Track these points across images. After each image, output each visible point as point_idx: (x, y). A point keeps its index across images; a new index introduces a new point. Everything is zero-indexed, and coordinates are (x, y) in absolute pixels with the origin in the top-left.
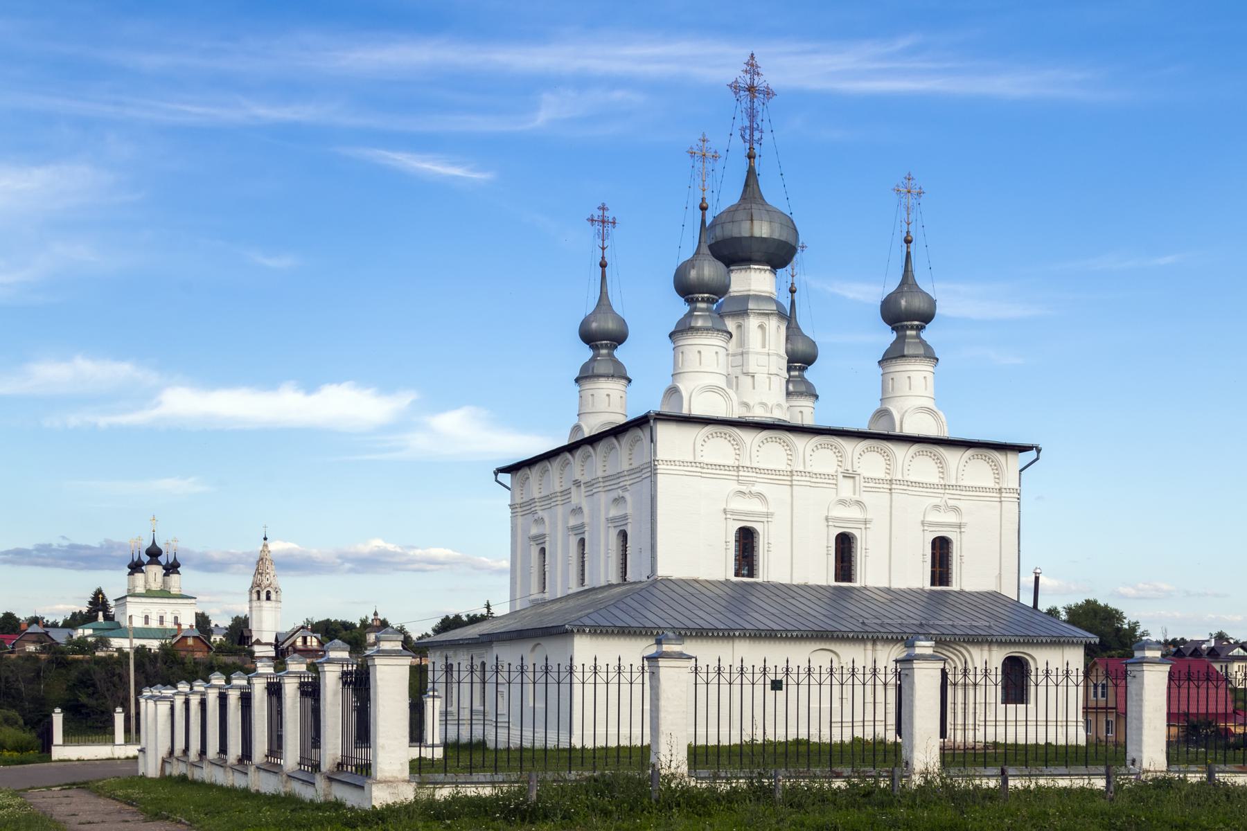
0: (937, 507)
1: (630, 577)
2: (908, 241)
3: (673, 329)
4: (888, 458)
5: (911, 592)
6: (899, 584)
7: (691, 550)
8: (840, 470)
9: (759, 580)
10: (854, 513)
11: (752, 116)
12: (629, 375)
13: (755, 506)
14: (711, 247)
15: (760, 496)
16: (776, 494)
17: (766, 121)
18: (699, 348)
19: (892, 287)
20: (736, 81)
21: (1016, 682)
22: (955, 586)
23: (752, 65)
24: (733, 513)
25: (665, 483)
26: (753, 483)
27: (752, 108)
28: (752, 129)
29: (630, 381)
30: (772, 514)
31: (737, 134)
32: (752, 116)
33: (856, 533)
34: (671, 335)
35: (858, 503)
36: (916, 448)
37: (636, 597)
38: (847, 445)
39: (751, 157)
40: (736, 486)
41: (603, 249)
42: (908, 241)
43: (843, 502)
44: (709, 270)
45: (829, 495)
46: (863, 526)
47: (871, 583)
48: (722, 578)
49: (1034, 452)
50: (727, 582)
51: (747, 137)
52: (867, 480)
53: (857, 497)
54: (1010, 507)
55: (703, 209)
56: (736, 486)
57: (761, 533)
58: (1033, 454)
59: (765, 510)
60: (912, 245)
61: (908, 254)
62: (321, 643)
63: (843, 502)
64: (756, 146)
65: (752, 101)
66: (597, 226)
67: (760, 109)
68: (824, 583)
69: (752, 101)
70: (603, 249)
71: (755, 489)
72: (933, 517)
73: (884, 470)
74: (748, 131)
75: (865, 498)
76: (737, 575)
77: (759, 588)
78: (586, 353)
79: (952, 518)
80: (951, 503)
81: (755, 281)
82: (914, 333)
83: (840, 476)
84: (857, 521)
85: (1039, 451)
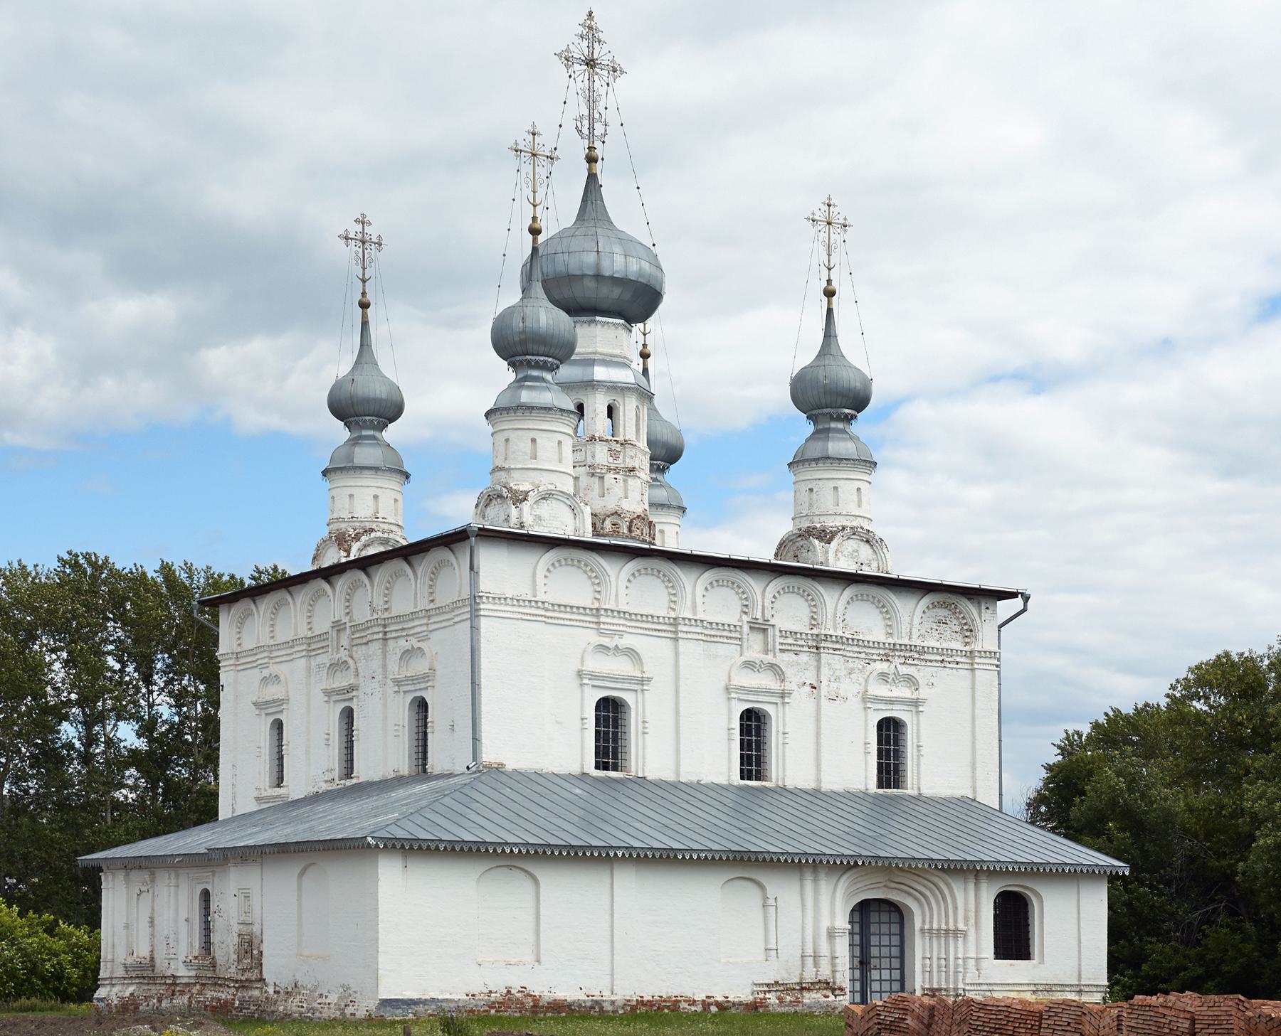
0: (883, 676)
1: (436, 762)
2: (829, 293)
3: (490, 406)
4: (597, 580)
5: (849, 796)
7: (530, 725)
9: (909, 792)
11: (592, 101)
12: (407, 468)
13: (620, 666)
14: (546, 284)
15: (631, 653)
16: (654, 650)
17: (612, 108)
18: (533, 434)
19: (344, 367)
20: (568, 50)
21: (1013, 936)
22: (910, 790)
23: (590, 28)
24: (593, 676)
25: (496, 632)
26: (621, 634)
27: (591, 89)
28: (591, 119)
29: (407, 476)
30: (649, 679)
31: (570, 126)
32: (592, 101)
33: (628, 698)
35: (772, 666)
36: (710, 575)
37: (457, 795)
38: (754, 584)
39: (591, 160)
40: (593, 638)
41: (364, 281)
42: (829, 293)
43: (749, 665)
44: (548, 317)
45: (728, 651)
46: (779, 700)
48: (576, 770)
49: (1019, 600)
51: (586, 131)
52: (785, 634)
53: (769, 658)
54: (985, 677)
55: (535, 232)
57: (632, 706)
58: (1017, 603)
60: (834, 299)
61: (830, 311)
62: (89, 934)
63: (749, 665)
64: (597, 144)
65: (591, 80)
66: (355, 248)
67: (603, 91)
68: (723, 781)
69: (591, 80)
70: (364, 281)
73: (807, 620)
74: (586, 123)
75: (783, 660)
77: (631, 785)
78: (339, 432)
79: (903, 692)
80: (904, 670)
81: (599, 337)
83: (746, 628)
84: (770, 693)
85: (1026, 598)
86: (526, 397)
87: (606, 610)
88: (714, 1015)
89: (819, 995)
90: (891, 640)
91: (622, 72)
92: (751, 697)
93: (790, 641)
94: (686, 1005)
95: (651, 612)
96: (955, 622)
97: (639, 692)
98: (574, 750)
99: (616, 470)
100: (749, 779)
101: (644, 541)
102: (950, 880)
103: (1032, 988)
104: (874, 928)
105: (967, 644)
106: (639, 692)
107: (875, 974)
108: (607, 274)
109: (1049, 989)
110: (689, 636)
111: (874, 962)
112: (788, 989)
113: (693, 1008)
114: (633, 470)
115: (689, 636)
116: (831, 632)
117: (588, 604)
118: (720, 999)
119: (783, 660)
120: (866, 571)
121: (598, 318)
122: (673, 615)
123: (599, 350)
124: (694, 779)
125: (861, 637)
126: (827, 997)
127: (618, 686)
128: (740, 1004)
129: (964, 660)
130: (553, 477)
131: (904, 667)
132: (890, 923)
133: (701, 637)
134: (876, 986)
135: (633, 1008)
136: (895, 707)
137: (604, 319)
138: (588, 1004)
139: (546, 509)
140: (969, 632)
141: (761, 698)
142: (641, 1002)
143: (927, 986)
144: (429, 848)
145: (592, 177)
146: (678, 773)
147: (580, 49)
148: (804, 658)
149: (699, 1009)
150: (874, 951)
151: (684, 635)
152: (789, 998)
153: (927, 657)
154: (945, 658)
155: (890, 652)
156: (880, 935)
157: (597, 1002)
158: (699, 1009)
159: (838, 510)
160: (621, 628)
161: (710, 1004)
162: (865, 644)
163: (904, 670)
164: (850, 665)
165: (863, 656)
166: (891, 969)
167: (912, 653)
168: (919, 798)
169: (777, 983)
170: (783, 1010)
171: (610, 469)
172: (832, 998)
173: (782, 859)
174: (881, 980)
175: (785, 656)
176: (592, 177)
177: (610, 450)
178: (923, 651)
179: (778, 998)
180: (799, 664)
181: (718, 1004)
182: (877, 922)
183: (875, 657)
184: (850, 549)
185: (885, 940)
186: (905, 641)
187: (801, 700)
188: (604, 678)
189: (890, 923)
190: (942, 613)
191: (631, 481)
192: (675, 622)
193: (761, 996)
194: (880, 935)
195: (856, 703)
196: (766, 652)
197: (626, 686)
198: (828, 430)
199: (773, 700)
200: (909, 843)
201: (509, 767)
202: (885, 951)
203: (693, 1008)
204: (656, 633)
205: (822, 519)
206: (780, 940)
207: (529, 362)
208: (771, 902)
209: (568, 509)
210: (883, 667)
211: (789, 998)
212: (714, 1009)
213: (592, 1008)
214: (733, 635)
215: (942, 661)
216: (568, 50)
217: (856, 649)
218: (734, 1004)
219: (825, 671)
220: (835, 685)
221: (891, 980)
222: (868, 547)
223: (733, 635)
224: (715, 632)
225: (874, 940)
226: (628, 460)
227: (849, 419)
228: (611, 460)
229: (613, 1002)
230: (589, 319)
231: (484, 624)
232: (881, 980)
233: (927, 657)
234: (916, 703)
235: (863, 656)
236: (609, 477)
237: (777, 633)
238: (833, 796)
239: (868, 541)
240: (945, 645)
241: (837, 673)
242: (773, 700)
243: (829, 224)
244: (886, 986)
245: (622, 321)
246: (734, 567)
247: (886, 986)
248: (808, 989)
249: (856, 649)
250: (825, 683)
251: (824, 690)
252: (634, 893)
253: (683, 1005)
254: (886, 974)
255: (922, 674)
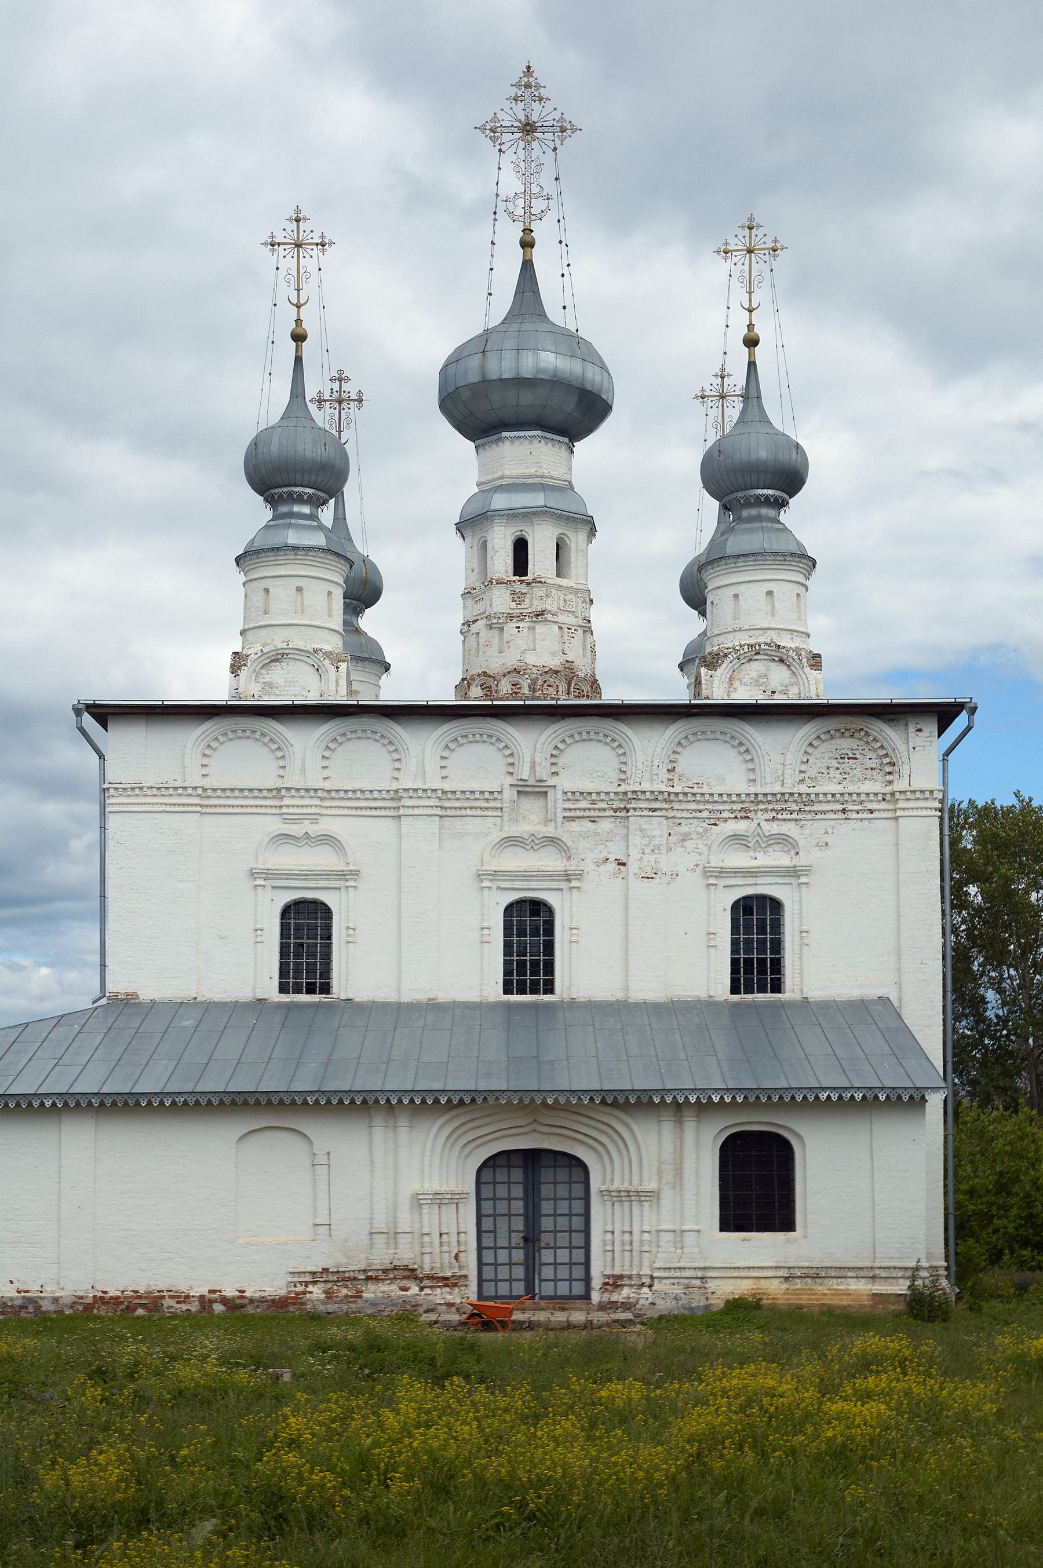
0: (738, 840)
2: (299, 338)
4: (280, 752)
6: (648, 987)
8: (510, 780)
10: (549, 861)
15: (327, 840)
20: (495, 119)
21: (757, 1187)
22: (791, 991)
23: (528, 86)
26: (315, 819)
30: (356, 873)
33: (551, 898)
34: (238, 560)
35: (553, 841)
39: (527, 244)
40: (274, 825)
45: (483, 831)
47: (816, 992)
50: (711, 1005)
53: (550, 830)
56: (274, 825)
59: (343, 867)
71: (314, 829)
72: (515, 861)
73: (615, 776)
75: (569, 832)
76: (732, 993)
79: (781, 859)
80: (775, 828)
82: (306, 510)
83: (509, 794)
84: (327, 874)
86: (735, 544)
87: (288, 789)
88: (221, 1317)
89: (394, 1287)
90: (752, 790)
91: (574, 130)
92: (517, 884)
93: (583, 804)
94: (173, 1303)
95: (358, 786)
96: (870, 755)
97: (343, 890)
98: (478, 972)
99: (521, 617)
100: (749, 990)
101: (552, 699)
102: (629, 1120)
103: (784, 1273)
104: (546, 1190)
105: (890, 782)
106: (566, 892)
107: (547, 1256)
108: (494, 378)
109: (815, 1275)
110: (417, 811)
111: (546, 1239)
112: (344, 1278)
113: (184, 1307)
114: (542, 613)
115: (417, 811)
116: (646, 786)
117: (271, 784)
118: (230, 1292)
119: (569, 832)
120: (779, 699)
121: (504, 434)
122: (395, 786)
123: (507, 473)
124: (422, 997)
125: (706, 789)
126: (406, 1289)
127: (311, 884)
128: (262, 1300)
129: (884, 805)
130: (285, 633)
131: (775, 824)
132: (570, 1183)
133: (163, 808)
134: (548, 1272)
135: (88, 1308)
136: (759, 881)
137: (513, 434)
138: (17, 1303)
139: (277, 674)
140: (890, 766)
141: (534, 885)
142: (101, 1300)
143: (608, 1272)
144: (281, 1102)
145: (527, 265)
146: (399, 991)
147: (512, 115)
148: (605, 825)
149: (194, 1307)
150: (546, 1223)
151: (410, 812)
152: (344, 1291)
153: (817, 807)
154: (845, 807)
155: (746, 806)
156: (555, 1199)
157: (31, 1300)
158: (194, 1307)
159: (738, 624)
160: (314, 810)
161: (212, 1301)
162: (709, 799)
163: (775, 828)
164: (684, 829)
165: (705, 814)
166: (571, 1248)
167: (779, 804)
168: (573, 1004)
169: (326, 1270)
170: (331, 1308)
171: (511, 617)
172: (414, 1289)
173: (823, 1096)
174: (555, 1264)
175: (575, 826)
176: (527, 265)
177: (513, 593)
178: (806, 800)
179: (326, 1292)
180: (597, 834)
181: (224, 1301)
182: (534, 1183)
183: (726, 815)
184: (754, 674)
185: (563, 1207)
186: (777, 788)
187: (601, 883)
188: (288, 876)
189: (570, 1183)
190: (846, 744)
191: (540, 628)
192: (396, 796)
193: (300, 1288)
194: (555, 1199)
195: (694, 881)
196: (546, 821)
197: (322, 884)
198: (291, 515)
199: (554, 885)
200: (580, 1067)
201: (146, 995)
202: (562, 1223)
203: (184, 1307)
204: (373, 812)
205: (721, 639)
206: (372, 1209)
207: (290, 494)
208: (322, 1159)
209: (312, 670)
210: (742, 826)
211: (344, 1291)
212: (218, 1308)
213: (23, 1307)
214: (492, 804)
215: (844, 811)
216: (495, 119)
217: (693, 806)
218: (252, 1300)
219: (636, 840)
220: (652, 858)
221: (571, 1264)
222: (783, 668)
223: (492, 804)
224: (451, 805)
225: (546, 1207)
226: (536, 603)
227: (780, 504)
228: (513, 605)
229: (56, 1300)
230: (496, 437)
231: (112, 821)
232: (555, 1264)
233: (817, 807)
234: (793, 872)
235: (705, 814)
236: (510, 627)
237: (559, 795)
238: (637, 1005)
239: (781, 661)
240: (851, 789)
241: (656, 842)
242: (554, 885)
243: (298, 245)
244: (563, 1272)
245: (539, 433)
246: (431, 715)
247: (563, 1272)
248: (376, 1279)
249: (693, 806)
250: (635, 854)
251: (633, 867)
252: (82, 1152)
253: (167, 1302)
254: (563, 1256)
255: (805, 833)
